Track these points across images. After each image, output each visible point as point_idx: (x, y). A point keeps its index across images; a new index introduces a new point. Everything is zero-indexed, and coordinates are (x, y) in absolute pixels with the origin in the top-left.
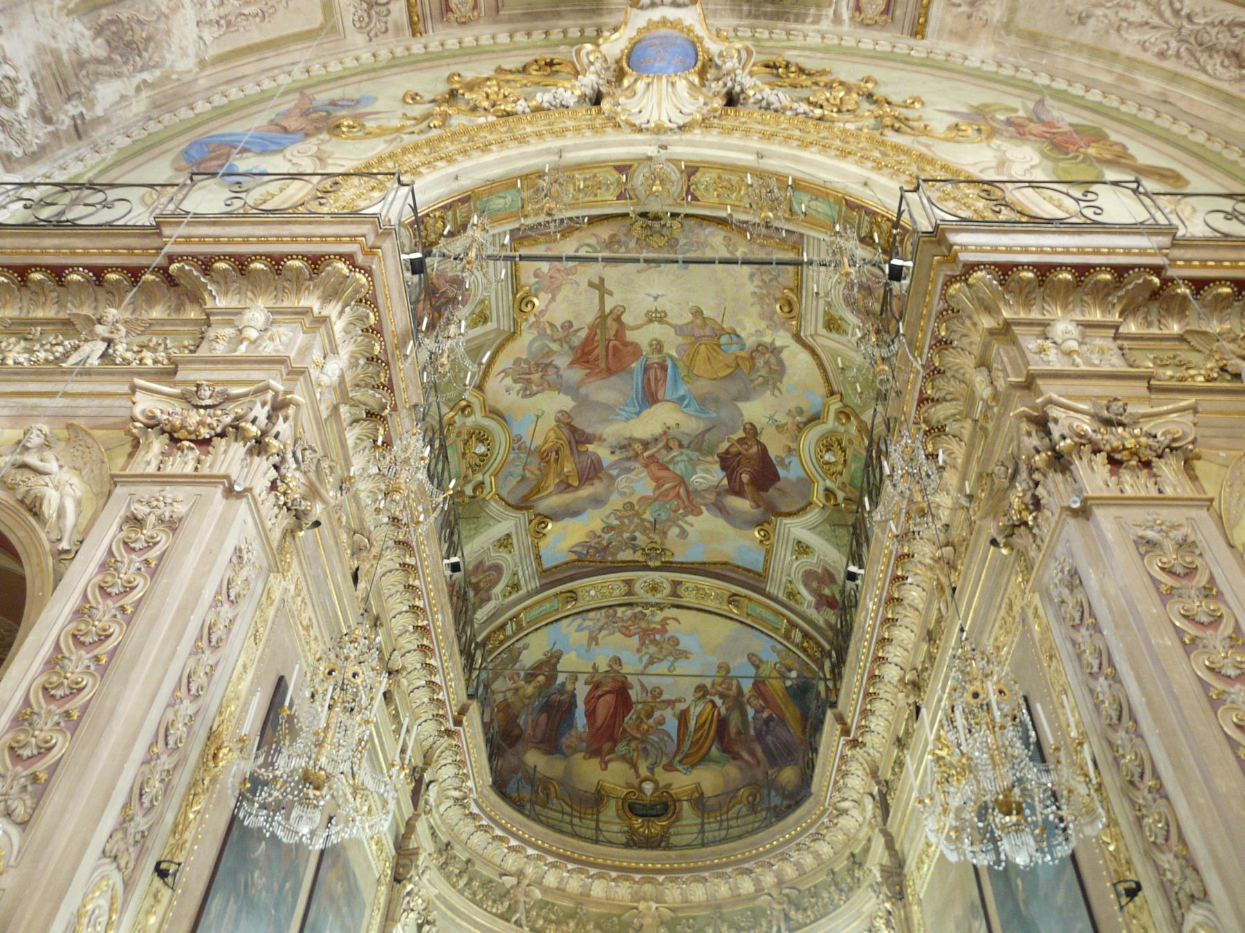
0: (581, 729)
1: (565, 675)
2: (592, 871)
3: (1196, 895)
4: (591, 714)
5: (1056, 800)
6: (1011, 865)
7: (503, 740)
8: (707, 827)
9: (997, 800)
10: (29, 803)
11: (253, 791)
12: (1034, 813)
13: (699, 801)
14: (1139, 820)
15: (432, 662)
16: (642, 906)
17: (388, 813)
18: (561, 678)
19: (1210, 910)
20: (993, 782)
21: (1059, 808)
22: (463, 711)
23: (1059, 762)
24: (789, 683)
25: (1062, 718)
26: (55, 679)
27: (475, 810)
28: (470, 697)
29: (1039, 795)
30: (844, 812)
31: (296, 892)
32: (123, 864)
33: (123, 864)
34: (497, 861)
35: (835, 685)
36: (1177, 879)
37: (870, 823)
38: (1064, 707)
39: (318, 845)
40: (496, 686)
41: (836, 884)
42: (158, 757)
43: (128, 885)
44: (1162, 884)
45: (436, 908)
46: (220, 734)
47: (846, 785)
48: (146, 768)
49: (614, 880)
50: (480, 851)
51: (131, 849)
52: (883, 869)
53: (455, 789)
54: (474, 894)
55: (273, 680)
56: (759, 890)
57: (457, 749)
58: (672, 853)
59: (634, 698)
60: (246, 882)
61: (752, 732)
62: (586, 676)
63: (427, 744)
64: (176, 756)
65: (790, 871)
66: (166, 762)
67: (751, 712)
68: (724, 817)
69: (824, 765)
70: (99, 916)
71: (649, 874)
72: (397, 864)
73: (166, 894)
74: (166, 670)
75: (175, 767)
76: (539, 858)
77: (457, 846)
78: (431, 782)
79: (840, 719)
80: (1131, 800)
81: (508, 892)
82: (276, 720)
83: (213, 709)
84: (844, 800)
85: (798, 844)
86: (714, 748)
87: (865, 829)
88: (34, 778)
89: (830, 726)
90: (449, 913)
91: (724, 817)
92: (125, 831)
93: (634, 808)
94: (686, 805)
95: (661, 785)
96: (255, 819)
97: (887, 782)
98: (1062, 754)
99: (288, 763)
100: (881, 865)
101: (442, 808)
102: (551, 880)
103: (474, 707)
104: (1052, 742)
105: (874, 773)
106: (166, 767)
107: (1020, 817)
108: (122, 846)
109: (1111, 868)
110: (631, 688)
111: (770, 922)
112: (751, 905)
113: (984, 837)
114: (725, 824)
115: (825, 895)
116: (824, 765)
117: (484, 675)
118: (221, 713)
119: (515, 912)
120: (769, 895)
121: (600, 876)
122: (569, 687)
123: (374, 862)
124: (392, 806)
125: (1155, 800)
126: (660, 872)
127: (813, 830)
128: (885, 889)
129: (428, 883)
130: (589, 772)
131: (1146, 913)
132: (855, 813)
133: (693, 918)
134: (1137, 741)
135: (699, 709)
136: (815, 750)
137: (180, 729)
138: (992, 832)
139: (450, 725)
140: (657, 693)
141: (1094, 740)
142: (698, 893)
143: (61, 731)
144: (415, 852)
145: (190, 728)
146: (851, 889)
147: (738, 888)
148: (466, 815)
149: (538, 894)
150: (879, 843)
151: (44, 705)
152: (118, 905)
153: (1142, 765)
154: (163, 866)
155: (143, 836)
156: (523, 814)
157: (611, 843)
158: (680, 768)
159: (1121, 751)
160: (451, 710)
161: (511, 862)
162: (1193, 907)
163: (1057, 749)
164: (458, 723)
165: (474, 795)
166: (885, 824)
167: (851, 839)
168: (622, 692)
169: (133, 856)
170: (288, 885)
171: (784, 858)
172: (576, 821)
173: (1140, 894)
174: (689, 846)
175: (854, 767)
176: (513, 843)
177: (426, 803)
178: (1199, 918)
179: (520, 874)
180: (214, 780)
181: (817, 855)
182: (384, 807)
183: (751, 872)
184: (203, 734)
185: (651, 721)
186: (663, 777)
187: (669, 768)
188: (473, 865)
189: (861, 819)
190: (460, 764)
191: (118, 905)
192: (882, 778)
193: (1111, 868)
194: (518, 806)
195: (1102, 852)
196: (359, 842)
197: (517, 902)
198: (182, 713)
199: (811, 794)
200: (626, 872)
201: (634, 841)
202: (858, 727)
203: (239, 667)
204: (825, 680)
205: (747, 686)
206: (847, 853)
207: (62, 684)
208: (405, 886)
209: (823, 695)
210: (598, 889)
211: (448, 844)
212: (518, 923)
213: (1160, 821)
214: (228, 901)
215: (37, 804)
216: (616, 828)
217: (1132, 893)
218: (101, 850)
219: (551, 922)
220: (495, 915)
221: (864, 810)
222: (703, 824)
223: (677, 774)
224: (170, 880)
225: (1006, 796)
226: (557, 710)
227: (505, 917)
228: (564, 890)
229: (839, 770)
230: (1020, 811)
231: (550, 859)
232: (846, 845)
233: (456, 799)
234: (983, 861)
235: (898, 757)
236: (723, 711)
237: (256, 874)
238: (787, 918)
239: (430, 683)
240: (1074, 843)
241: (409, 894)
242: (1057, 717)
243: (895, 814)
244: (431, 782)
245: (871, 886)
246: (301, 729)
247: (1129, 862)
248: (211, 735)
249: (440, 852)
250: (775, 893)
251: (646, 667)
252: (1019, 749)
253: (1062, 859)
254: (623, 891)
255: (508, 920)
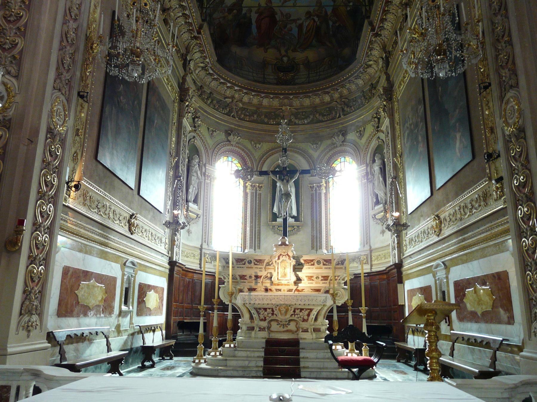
0: (254, 34)
1: (246, 9)
2: (263, 95)
3: (513, 85)
4: (259, 27)
5: (462, 48)
6: (437, 77)
7: (220, 42)
8: (311, 75)
9: (436, 49)
10: (16, 68)
11: (110, 60)
12: (451, 53)
13: (307, 64)
14: (497, 56)
15: (184, 4)
16: (284, 108)
17: (170, 66)
18: (244, 11)
19: (517, 91)
20: (434, 40)
21: (462, 52)
22: (201, 27)
23: (466, 30)
24: (349, 9)
25: (473, 14)
26: (7, 12)
27: (211, 72)
28: (203, 20)
29: (454, 45)
30: (370, 66)
31: (140, 104)
32: (64, 92)
33: (64, 92)
34: (223, 92)
35: (370, 8)
36: (507, 80)
37: (380, 70)
38: (474, 8)
39: (144, 81)
40: (215, 16)
41: (364, 97)
42: (66, 48)
43: (68, 100)
44: (500, 82)
45: (200, 112)
46: (91, 37)
47: (371, 54)
48: (61, 52)
49: (272, 98)
50: (215, 89)
51: (65, 87)
52: (384, 89)
53: (201, 63)
54: (214, 106)
55: (109, 13)
56: (332, 100)
57: (200, 45)
58: (296, 87)
59: (278, 19)
60: (118, 101)
61: (331, 33)
62: (256, 9)
63: (186, 43)
64: (74, 47)
65: (345, 92)
66: (70, 50)
67: (331, 23)
68: (318, 71)
69: (362, 45)
70: (60, 112)
71: (286, 95)
72: (181, 95)
73: (86, 105)
74: (57, 6)
75: (74, 52)
76: (240, 91)
77: (205, 87)
78: (190, 60)
79: (371, 23)
80: (495, 47)
81: (228, 105)
82: (116, 30)
83: (85, 25)
84: (370, 61)
85: (349, 81)
86: (314, 41)
87: (378, 73)
88: (14, 57)
89: (366, 28)
90: (205, 114)
91: (318, 71)
92: (60, 79)
93: (280, 68)
94: (301, 66)
95: (291, 58)
96: (114, 72)
97: (389, 52)
98: (469, 27)
99: (122, 46)
100: (383, 87)
101: (197, 72)
102: (246, 99)
103: (205, 25)
104: (465, 20)
105: (384, 48)
106: (71, 52)
107: (444, 56)
108: (61, 85)
109: (480, 79)
110: (277, 14)
111: (336, 112)
112: (328, 106)
113: (428, 66)
114: (318, 74)
115: (359, 101)
116: (362, 45)
117: (208, 11)
118: (89, 28)
119: (232, 113)
120: (336, 101)
121: (266, 97)
122: (248, 15)
123: (170, 91)
124: (171, 63)
125: (506, 46)
126: (291, 94)
127: (356, 75)
128: (384, 97)
129: (194, 102)
130: (259, 54)
131: (490, 95)
132: (374, 66)
133: (305, 112)
134: (505, 20)
135: (307, 23)
136: (359, 39)
137: (72, 35)
138: (431, 64)
139: (196, 34)
140: (288, 15)
141: (485, 22)
142: (307, 102)
143: (18, 36)
144: (188, 89)
145: (76, 34)
146: (370, 98)
147: (323, 100)
148: (207, 74)
149: (241, 105)
150: (384, 77)
151: (7, 25)
152: (67, 108)
153: (504, 32)
154: (81, 94)
155: (69, 81)
156: (232, 73)
157: (270, 83)
158: (299, 50)
159: (497, 26)
160: (195, 27)
161: (228, 93)
162: (510, 91)
163: (467, 24)
164: (199, 33)
165: (210, 65)
166: (387, 69)
167: (371, 77)
168: (272, 15)
169: (67, 89)
170: (136, 102)
171: (343, 86)
172: (254, 75)
173: (490, 88)
174: (303, 83)
175: (376, 46)
176: (229, 85)
177: (190, 69)
178: (512, 94)
179: (233, 97)
180: (94, 59)
181: (357, 85)
182: (168, 64)
183: (329, 93)
184: (83, 38)
185: (286, 29)
186: (292, 55)
187: (294, 50)
188: (213, 94)
189: (376, 69)
190: (202, 52)
191: (67, 108)
192: (387, 50)
193: (480, 79)
194: (230, 70)
195: (477, 72)
196: (158, 79)
197: (232, 108)
198: (70, 27)
199: (356, 59)
200: (276, 95)
201: (280, 82)
202: (379, 27)
203: (92, 6)
204: (365, 6)
205: (329, 10)
206: (370, 83)
207: (11, 15)
208: (185, 103)
209: (364, 13)
210: (265, 102)
211: (201, 86)
212: (233, 116)
213: (506, 56)
214: (112, 109)
215: (19, 68)
216: (272, 77)
217: (486, 88)
218: (52, 88)
219: (247, 115)
220: (224, 114)
221: (378, 65)
222: (309, 74)
223: (298, 53)
224: (85, 99)
225: (439, 48)
226: (243, 25)
227: (228, 114)
228: (251, 103)
229: (369, 47)
230: (445, 54)
231: (245, 91)
232: (369, 80)
233: (203, 68)
234: (426, 76)
235: (395, 40)
236: (318, 23)
237: (121, 98)
238: (343, 110)
239: (184, 15)
240: (466, 67)
241: (187, 106)
242: (471, 13)
243: (392, 65)
244: (190, 60)
245: (379, 96)
246: (126, 32)
247: (488, 75)
248: (88, 38)
249: (198, 90)
250: (338, 101)
251: (283, 3)
252: (450, 27)
253: (459, 74)
254: (276, 103)
255: (229, 116)
